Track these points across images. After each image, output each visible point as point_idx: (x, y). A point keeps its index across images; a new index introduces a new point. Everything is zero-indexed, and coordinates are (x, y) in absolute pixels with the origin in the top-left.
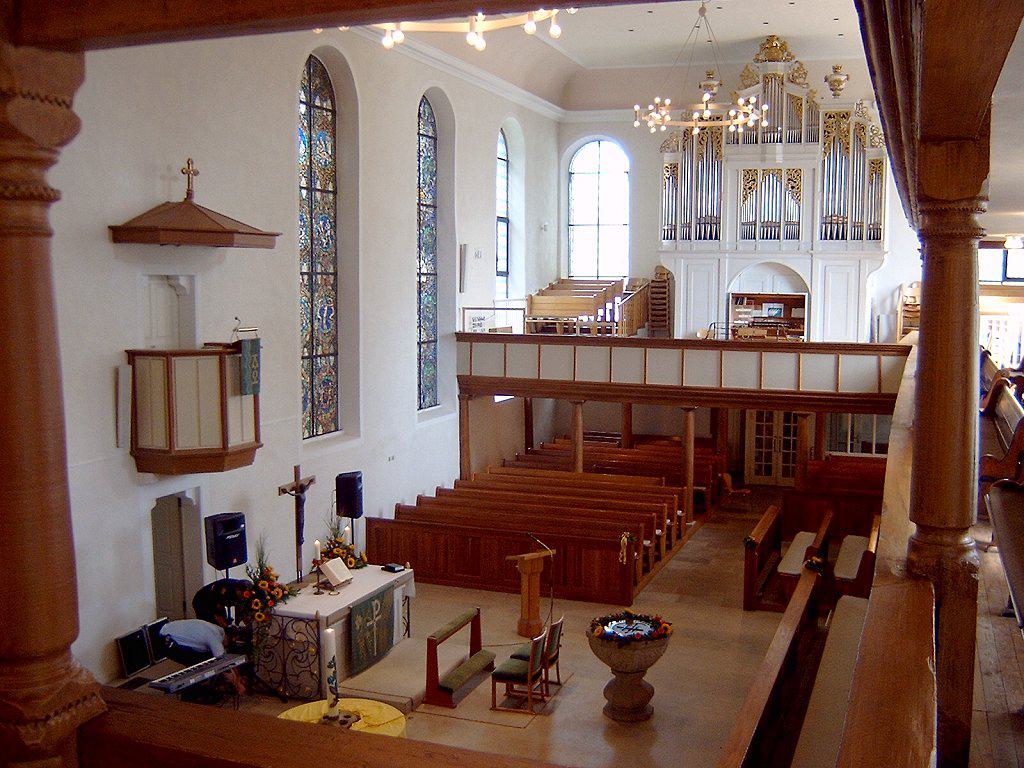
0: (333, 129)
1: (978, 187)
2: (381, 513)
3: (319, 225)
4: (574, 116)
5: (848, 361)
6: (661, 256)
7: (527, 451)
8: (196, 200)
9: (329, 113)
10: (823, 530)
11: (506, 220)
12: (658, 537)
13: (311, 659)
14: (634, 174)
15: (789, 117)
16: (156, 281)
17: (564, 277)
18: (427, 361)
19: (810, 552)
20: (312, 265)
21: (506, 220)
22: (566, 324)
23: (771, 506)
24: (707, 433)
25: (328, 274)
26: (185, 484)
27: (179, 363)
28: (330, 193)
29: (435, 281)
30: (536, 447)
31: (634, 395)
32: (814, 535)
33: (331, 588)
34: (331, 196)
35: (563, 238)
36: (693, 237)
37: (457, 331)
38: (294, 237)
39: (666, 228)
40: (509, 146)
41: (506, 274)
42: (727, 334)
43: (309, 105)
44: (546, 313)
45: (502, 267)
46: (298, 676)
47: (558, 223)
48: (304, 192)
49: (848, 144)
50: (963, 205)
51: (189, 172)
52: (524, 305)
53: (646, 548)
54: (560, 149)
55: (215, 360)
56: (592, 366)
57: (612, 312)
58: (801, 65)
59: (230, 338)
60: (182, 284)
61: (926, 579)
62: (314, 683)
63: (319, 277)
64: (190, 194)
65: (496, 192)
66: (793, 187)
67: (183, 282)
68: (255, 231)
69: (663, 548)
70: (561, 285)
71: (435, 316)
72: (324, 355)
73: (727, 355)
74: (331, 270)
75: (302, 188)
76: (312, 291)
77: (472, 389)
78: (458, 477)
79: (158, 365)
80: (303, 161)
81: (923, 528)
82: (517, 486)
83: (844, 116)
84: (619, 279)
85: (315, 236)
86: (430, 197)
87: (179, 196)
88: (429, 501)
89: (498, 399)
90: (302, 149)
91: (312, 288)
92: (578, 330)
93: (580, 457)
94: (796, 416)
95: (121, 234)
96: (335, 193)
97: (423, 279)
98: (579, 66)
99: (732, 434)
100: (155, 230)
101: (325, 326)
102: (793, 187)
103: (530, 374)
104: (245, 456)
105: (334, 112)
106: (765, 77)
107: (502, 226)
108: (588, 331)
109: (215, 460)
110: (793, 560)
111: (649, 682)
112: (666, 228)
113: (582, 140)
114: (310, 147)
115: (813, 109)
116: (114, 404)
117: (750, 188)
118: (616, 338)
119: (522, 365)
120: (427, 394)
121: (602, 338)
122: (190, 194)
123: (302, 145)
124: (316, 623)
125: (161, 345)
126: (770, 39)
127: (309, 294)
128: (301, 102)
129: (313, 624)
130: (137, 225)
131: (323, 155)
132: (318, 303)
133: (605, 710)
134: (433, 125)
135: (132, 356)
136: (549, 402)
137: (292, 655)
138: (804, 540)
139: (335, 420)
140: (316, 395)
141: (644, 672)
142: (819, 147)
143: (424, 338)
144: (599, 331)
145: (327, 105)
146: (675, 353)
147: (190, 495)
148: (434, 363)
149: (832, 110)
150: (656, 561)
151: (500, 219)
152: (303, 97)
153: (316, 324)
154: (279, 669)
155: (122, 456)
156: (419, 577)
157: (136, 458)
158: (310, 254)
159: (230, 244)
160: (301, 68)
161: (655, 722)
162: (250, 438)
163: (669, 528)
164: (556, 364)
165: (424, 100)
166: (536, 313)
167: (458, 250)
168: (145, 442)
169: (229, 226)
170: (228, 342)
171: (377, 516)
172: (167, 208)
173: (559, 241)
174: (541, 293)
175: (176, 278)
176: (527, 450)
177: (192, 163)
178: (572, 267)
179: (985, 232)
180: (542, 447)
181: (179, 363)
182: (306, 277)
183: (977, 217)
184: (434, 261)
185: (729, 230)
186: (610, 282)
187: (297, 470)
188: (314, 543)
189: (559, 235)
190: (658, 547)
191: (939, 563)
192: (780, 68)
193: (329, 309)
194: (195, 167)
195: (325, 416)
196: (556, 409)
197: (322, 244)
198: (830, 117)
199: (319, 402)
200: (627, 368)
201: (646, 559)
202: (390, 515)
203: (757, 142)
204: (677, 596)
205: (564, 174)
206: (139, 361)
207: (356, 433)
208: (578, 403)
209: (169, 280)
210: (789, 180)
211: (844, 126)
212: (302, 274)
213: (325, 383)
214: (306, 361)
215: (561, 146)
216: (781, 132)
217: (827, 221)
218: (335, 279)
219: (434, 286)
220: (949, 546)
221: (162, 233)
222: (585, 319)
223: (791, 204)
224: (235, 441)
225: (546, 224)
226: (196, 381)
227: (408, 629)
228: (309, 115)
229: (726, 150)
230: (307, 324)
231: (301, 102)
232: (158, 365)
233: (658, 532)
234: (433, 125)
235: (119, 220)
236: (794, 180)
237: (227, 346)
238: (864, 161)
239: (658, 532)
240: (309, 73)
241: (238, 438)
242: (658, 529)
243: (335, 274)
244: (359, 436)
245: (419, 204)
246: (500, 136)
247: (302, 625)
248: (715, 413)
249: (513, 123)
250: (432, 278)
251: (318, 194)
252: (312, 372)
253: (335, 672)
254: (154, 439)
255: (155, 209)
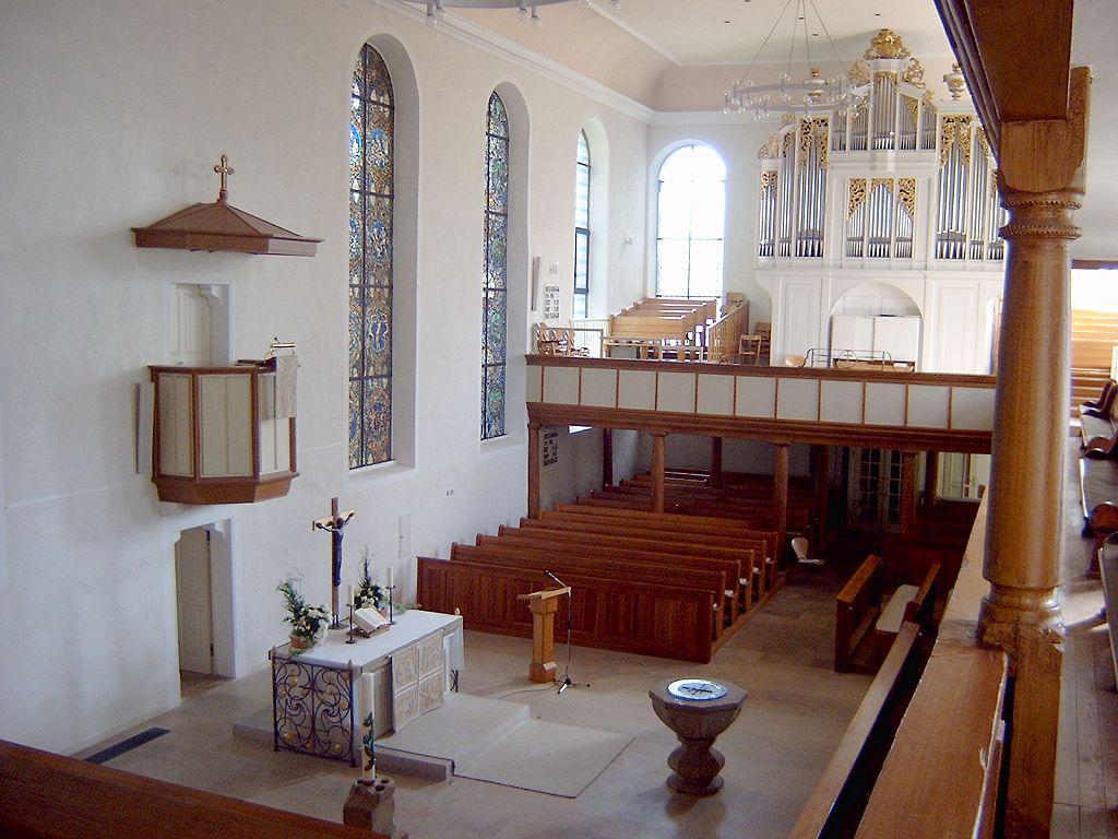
0: (390, 125)
1: (1070, 175)
2: (437, 553)
3: (372, 233)
4: (665, 118)
5: (960, 392)
6: (758, 272)
7: (604, 489)
8: (230, 202)
9: (386, 109)
10: (927, 586)
11: (587, 232)
12: (743, 587)
13: (343, 713)
14: (734, 185)
15: (903, 119)
16: (186, 291)
17: (651, 295)
18: (493, 385)
19: (910, 606)
20: (364, 277)
21: (587, 232)
22: (650, 348)
23: (871, 556)
24: (803, 470)
25: (382, 287)
26: (212, 515)
27: (206, 381)
28: (384, 199)
29: (504, 297)
30: (616, 483)
31: (721, 428)
32: (918, 588)
33: (366, 636)
34: (387, 201)
35: (651, 256)
36: (793, 253)
37: (528, 353)
38: (340, 246)
39: (763, 242)
40: (591, 150)
41: (586, 291)
42: (829, 362)
43: (364, 99)
44: (630, 336)
45: (581, 283)
46: (328, 732)
47: (656, 236)
48: (356, 196)
49: (968, 151)
50: (1053, 198)
51: (223, 170)
52: (605, 326)
53: (728, 599)
54: (649, 154)
55: (245, 380)
56: (675, 395)
57: (703, 335)
58: (917, 62)
59: (263, 357)
60: (213, 293)
61: (1000, 649)
62: (345, 740)
63: (372, 290)
64: (223, 195)
65: (573, 194)
66: (905, 200)
67: (215, 292)
68: (296, 237)
69: (748, 599)
70: (648, 306)
71: (504, 335)
72: (376, 376)
73: (827, 384)
74: (386, 283)
75: (353, 191)
76: (364, 307)
77: (545, 420)
78: (525, 513)
79: (183, 383)
80: (356, 161)
81: (998, 588)
82: (587, 526)
83: (964, 120)
84: (712, 299)
85: (368, 244)
86: (500, 203)
87: (212, 197)
88: (490, 540)
89: (573, 429)
90: (355, 149)
91: (363, 300)
92: (701, 357)
93: (660, 495)
94: (904, 454)
95: (146, 237)
96: (391, 197)
97: (491, 295)
98: (671, 62)
99: (832, 470)
100: (181, 233)
101: (378, 346)
102: (905, 200)
103: (607, 402)
104: (279, 486)
105: (392, 108)
106: (877, 76)
107: (582, 239)
108: (674, 356)
109: (242, 490)
110: (892, 618)
111: (719, 749)
112: (763, 242)
113: (668, 149)
114: (365, 146)
115: (930, 113)
116: (134, 424)
117: (857, 200)
118: (703, 364)
119: (598, 392)
120: (493, 423)
121: (689, 365)
122: (223, 195)
123: (356, 145)
124: (348, 673)
125: (188, 361)
126: (883, 33)
127: (360, 309)
128: (354, 96)
129: (345, 675)
130: (161, 227)
131: (378, 156)
132: (371, 319)
133: (670, 782)
134: (505, 124)
135: (156, 372)
136: (631, 435)
137: (323, 707)
138: (906, 594)
139: (388, 448)
140: (365, 420)
141: (712, 740)
142: (936, 154)
143: (490, 360)
144: (687, 357)
145: (385, 99)
146: (770, 381)
147: (218, 528)
148: (501, 388)
149: (952, 114)
150: (739, 614)
151: (579, 230)
152: (357, 91)
153: (367, 341)
154: (308, 722)
155: (142, 482)
156: (468, 624)
157: (158, 486)
158: (361, 264)
159: (263, 250)
160: (354, 61)
161: (723, 795)
162: (284, 466)
163: (756, 576)
164: (637, 392)
165: (495, 97)
166: (618, 336)
167: (530, 262)
168: (169, 468)
169: (263, 230)
170: (262, 359)
171: (433, 557)
172: (199, 209)
173: (646, 257)
174: (625, 313)
175: (208, 287)
176: (604, 485)
177: (227, 160)
178: (660, 286)
179: (1079, 232)
180: (621, 482)
181: (206, 381)
182: (357, 290)
183: (1069, 213)
184: (504, 275)
185: (833, 245)
186: (701, 302)
187: (334, 503)
188: (351, 581)
189: (646, 249)
190: (742, 598)
191: (1016, 631)
192: (894, 66)
193: (383, 326)
194: (230, 164)
195: (376, 444)
196: (640, 440)
197: (375, 254)
198: (949, 121)
199: (370, 428)
200: (717, 397)
201: (727, 611)
202: (446, 556)
203: (865, 148)
204: (760, 654)
205: (652, 182)
206: (164, 379)
207: (411, 464)
208: (658, 436)
209: (200, 292)
210: (901, 191)
211: (964, 132)
212: (352, 286)
213: (377, 407)
214: (355, 383)
215: (649, 153)
216: (894, 137)
217: (946, 238)
218: (391, 293)
219: (504, 303)
220: (1028, 609)
221: (188, 236)
222: (673, 343)
223: (904, 220)
224: (267, 469)
225: (632, 236)
226: (223, 400)
227: (455, 683)
228: (364, 111)
229: (831, 155)
230: (357, 342)
231: (354, 96)
232: (183, 383)
233: (743, 581)
234: (505, 124)
235: (135, 227)
236: (907, 190)
237: (261, 364)
238: (986, 170)
239: (743, 581)
240: (364, 65)
241: (272, 463)
242: (744, 577)
243: (391, 287)
244: (414, 467)
245: (487, 212)
246: (581, 139)
247: (333, 675)
248: (717, 442)
249: (598, 128)
250: (501, 293)
251: (372, 198)
252: (362, 395)
253: (371, 731)
254: (177, 465)
255: (183, 211)
